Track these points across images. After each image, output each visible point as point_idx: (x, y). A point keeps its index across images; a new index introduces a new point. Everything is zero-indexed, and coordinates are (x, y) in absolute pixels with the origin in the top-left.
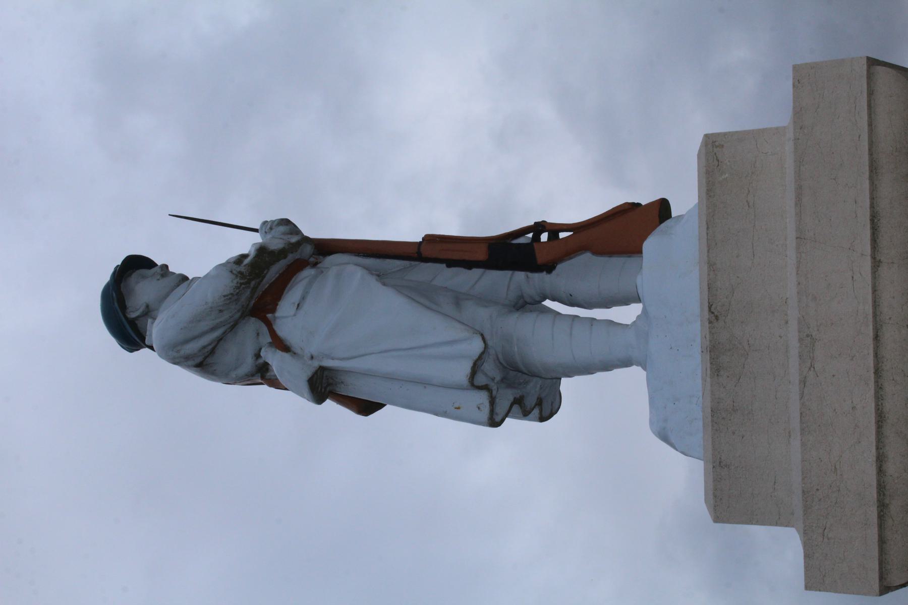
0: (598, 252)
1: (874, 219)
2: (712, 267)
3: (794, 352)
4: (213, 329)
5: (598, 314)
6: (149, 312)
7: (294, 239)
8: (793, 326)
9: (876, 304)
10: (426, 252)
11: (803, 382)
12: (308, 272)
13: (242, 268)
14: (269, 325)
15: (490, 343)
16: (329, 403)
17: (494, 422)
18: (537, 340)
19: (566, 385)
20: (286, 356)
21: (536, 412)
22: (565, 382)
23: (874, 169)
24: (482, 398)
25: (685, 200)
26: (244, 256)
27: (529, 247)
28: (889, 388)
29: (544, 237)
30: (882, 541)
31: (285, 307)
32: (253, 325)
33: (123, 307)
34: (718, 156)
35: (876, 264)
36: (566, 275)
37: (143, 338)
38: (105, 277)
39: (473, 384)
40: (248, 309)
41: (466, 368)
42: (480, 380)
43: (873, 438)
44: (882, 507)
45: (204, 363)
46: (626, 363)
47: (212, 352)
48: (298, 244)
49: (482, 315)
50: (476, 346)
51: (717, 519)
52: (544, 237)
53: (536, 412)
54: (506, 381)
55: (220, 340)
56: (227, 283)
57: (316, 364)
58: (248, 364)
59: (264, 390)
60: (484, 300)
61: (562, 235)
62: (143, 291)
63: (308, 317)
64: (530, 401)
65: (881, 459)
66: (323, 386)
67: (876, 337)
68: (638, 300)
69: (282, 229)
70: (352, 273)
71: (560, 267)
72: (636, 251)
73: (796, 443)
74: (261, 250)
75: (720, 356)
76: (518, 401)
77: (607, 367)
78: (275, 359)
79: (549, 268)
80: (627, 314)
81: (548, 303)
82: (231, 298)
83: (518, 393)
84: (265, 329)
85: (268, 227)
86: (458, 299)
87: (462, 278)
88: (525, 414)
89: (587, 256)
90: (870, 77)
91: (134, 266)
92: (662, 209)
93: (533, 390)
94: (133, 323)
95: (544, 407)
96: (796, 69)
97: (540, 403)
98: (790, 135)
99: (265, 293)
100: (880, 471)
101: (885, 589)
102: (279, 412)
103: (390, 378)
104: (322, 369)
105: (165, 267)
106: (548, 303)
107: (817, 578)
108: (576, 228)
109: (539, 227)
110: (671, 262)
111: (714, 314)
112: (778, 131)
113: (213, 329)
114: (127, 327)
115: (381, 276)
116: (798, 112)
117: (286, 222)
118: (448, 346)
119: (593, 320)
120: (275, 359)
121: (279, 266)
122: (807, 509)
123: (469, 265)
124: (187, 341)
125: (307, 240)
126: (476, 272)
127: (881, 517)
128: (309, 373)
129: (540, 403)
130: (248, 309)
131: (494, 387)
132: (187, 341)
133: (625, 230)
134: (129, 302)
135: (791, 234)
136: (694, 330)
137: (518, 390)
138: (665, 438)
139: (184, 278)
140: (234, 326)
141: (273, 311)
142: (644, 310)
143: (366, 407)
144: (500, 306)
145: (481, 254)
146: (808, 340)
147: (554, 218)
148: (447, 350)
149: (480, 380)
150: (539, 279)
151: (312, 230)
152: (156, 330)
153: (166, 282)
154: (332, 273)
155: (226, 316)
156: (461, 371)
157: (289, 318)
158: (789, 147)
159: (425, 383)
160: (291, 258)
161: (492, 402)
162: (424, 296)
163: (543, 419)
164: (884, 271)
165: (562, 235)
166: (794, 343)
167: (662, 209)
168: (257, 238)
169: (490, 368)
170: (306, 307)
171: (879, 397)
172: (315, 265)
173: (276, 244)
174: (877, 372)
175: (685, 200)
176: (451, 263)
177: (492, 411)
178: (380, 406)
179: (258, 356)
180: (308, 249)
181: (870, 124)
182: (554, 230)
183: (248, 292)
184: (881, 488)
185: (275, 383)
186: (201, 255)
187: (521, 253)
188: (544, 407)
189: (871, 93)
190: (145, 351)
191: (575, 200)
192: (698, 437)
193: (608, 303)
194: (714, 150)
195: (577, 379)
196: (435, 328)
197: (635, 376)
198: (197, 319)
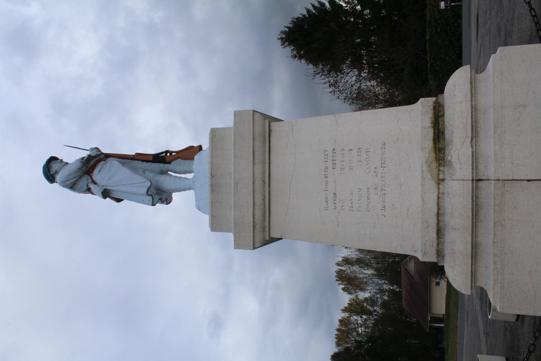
0: (182, 159)
1: (254, 152)
2: (212, 163)
3: (233, 187)
4: (74, 178)
5: (183, 176)
6: (56, 173)
7: (99, 153)
8: (233, 180)
9: (253, 174)
10: (135, 158)
11: (235, 195)
12: (102, 162)
13: (83, 161)
14: (91, 177)
15: (153, 183)
16: (108, 199)
17: (153, 205)
18: (165, 182)
19: (175, 195)
20: (96, 185)
21: (165, 202)
22: (173, 194)
23: (254, 139)
24: (150, 198)
25: (206, 146)
26: (84, 157)
27: (164, 157)
28: (256, 196)
29: (168, 154)
30: (254, 236)
31: (96, 172)
32: (86, 177)
33: (49, 171)
34: (214, 133)
35: (254, 164)
36: (175, 165)
37: (54, 179)
38: (44, 162)
39: (147, 194)
40: (87, 172)
41: (146, 190)
42: (150, 193)
43: (252, 209)
44: (254, 227)
45: (72, 187)
46: (190, 189)
47: (75, 184)
48: (99, 155)
49: (151, 175)
50: (149, 184)
51: (212, 230)
52: (168, 154)
53: (165, 202)
54: (157, 194)
55: (77, 181)
56: (79, 165)
57: (104, 188)
58: (85, 188)
59: (89, 195)
60: (152, 171)
61: (173, 154)
62: (55, 166)
63: (102, 175)
64: (164, 199)
65: (254, 215)
66: (106, 194)
67: (253, 183)
68: (193, 172)
69: (96, 150)
70: (114, 162)
71: (172, 163)
72: (192, 159)
73: (233, 210)
74: (89, 156)
75: (214, 188)
76: (160, 199)
77: (184, 190)
78: (92, 186)
79: (169, 163)
80: (190, 176)
81: (169, 172)
82: (80, 169)
83: (160, 197)
84: (90, 178)
85: (92, 149)
86: (144, 171)
87: (145, 165)
88: (162, 202)
89: (180, 160)
90: (253, 115)
91: (53, 159)
92: (200, 148)
93: (164, 197)
94: (52, 176)
95: (167, 201)
96: (235, 112)
97: (166, 199)
98: (233, 129)
99: (90, 168)
100: (254, 218)
101: (254, 248)
102: (94, 201)
103: (124, 192)
104: (106, 189)
105: (62, 160)
106: (169, 172)
107: (237, 246)
108: (177, 152)
109: (167, 152)
110: (201, 161)
111: (212, 176)
112: (230, 128)
113: (74, 178)
114: (50, 176)
115: (123, 164)
116: (235, 123)
117: (97, 148)
118: (141, 184)
119: (176, 176)
120: (92, 186)
121: (93, 162)
122: (235, 227)
123: (148, 161)
124: (67, 181)
125: (103, 153)
126: (150, 163)
127: (254, 230)
128: (102, 190)
129: (166, 199)
130: (87, 172)
131: (153, 195)
132: (67, 181)
133: (190, 153)
134: (51, 169)
135: (233, 155)
136: (207, 180)
137: (160, 196)
138: (199, 209)
139: (67, 163)
140: (81, 177)
141: (92, 173)
142: (195, 175)
143: (119, 200)
144: (157, 173)
145: (151, 159)
146: (236, 183)
147: (171, 149)
148: (140, 184)
149: (150, 193)
150: (167, 166)
151: (105, 151)
152: (58, 178)
153: (62, 164)
154: (110, 162)
155: (78, 174)
156: (144, 190)
157: (96, 175)
158: (233, 133)
159: (134, 194)
160: (98, 158)
161: (153, 199)
162: (135, 170)
163: (167, 204)
164: (256, 165)
165: (173, 154)
166: (233, 184)
167: (200, 148)
168: (88, 153)
169: (153, 190)
170: (101, 172)
171: (254, 199)
172: (104, 160)
173: (93, 154)
174: (253, 192)
175: (206, 146)
176: (143, 161)
177: (153, 202)
178: (122, 200)
179: (88, 186)
180: (103, 156)
181: (253, 127)
182: (171, 153)
183: (85, 167)
184: (254, 222)
185: (92, 193)
186: (72, 157)
187: (161, 159)
188: (167, 201)
189: (254, 119)
190: (55, 183)
191: (178, 144)
192: (208, 208)
193: (185, 173)
194: (213, 132)
195: (176, 193)
196: (138, 178)
197: (192, 192)
198: (70, 175)
